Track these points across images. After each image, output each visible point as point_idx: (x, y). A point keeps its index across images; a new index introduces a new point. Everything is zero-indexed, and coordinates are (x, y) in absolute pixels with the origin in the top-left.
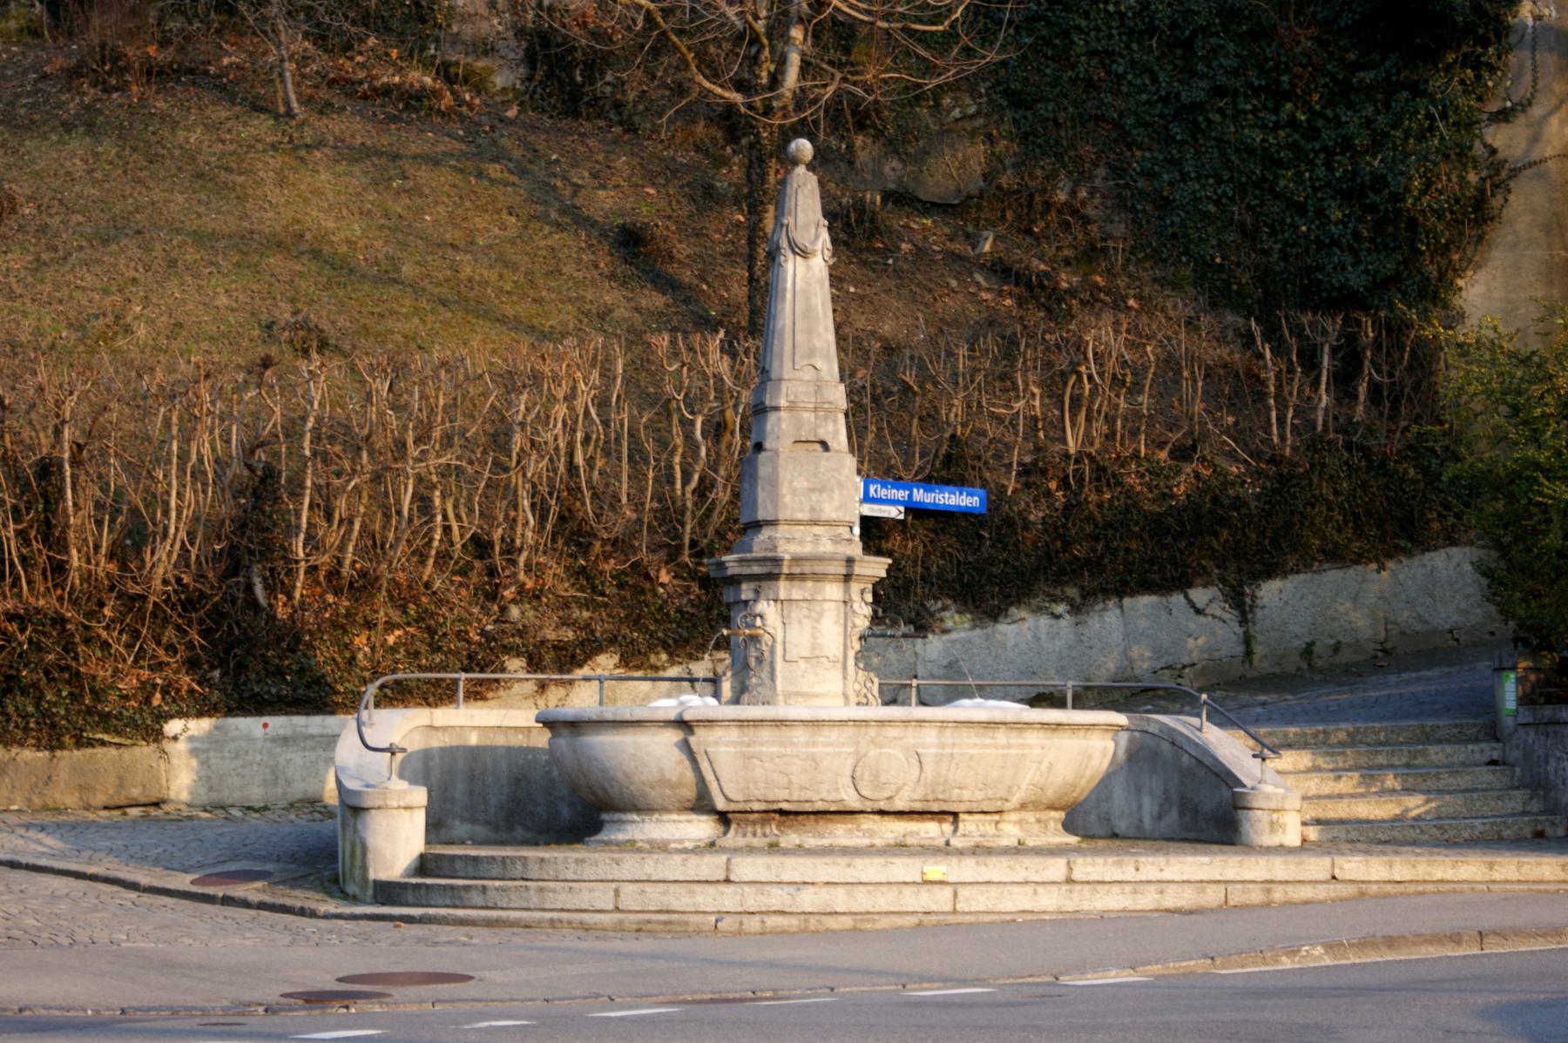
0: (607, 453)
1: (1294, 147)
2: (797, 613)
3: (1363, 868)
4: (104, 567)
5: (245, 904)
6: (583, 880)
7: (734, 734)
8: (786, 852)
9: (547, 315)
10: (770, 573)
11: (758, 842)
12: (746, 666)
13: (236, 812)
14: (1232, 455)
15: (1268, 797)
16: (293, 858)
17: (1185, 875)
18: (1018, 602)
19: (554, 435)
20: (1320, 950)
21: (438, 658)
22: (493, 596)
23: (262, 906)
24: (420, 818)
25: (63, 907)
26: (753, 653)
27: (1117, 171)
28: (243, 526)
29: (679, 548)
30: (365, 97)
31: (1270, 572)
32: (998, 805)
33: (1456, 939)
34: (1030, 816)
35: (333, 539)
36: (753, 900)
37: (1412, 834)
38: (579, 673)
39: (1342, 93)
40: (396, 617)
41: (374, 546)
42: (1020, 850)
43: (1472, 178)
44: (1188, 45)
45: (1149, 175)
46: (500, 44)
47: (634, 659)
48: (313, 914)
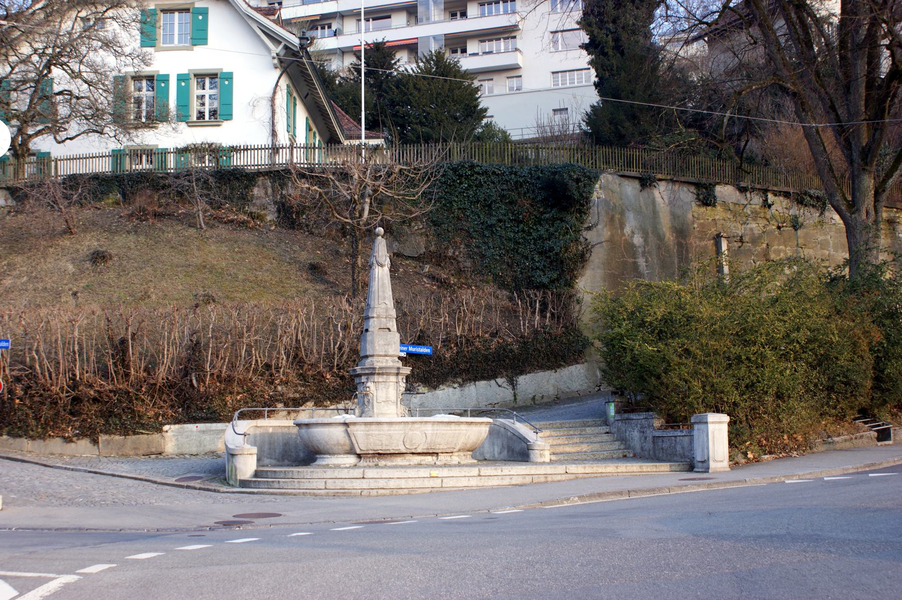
0: (309, 336)
1: (524, 238)
2: (381, 386)
3: (574, 469)
4: (143, 374)
5: (195, 488)
6: (312, 478)
7: (363, 427)
8: (382, 468)
9: (287, 292)
10: (372, 373)
11: (371, 464)
12: (364, 404)
13: (187, 456)
14: (508, 336)
15: (539, 446)
16: (210, 472)
17: (517, 472)
18: (443, 384)
19: (292, 330)
20: (576, 499)
21: (254, 404)
22: (272, 383)
23: (200, 489)
24: (255, 457)
25: (132, 490)
26: (366, 400)
27: (468, 246)
28: (189, 360)
29: (333, 367)
30: (225, 223)
31: (522, 373)
32: (451, 450)
33: (621, 493)
34: (461, 454)
35: (219, 364)
36: (373, 485)
37: (584, 457)
38: (301, 408)
39: (539, 221)
40: (240, 390)
41: (232, 366)
42: (459, 465)
43: (580, 248)
44: (490, 206)
45: (478, 247)
46: (269, 207)
47: (319, 404)
48: (219, 491)
